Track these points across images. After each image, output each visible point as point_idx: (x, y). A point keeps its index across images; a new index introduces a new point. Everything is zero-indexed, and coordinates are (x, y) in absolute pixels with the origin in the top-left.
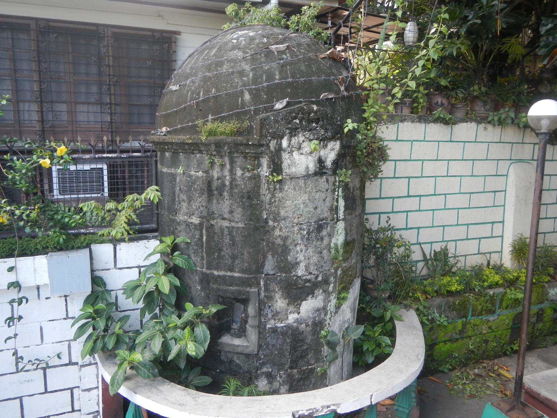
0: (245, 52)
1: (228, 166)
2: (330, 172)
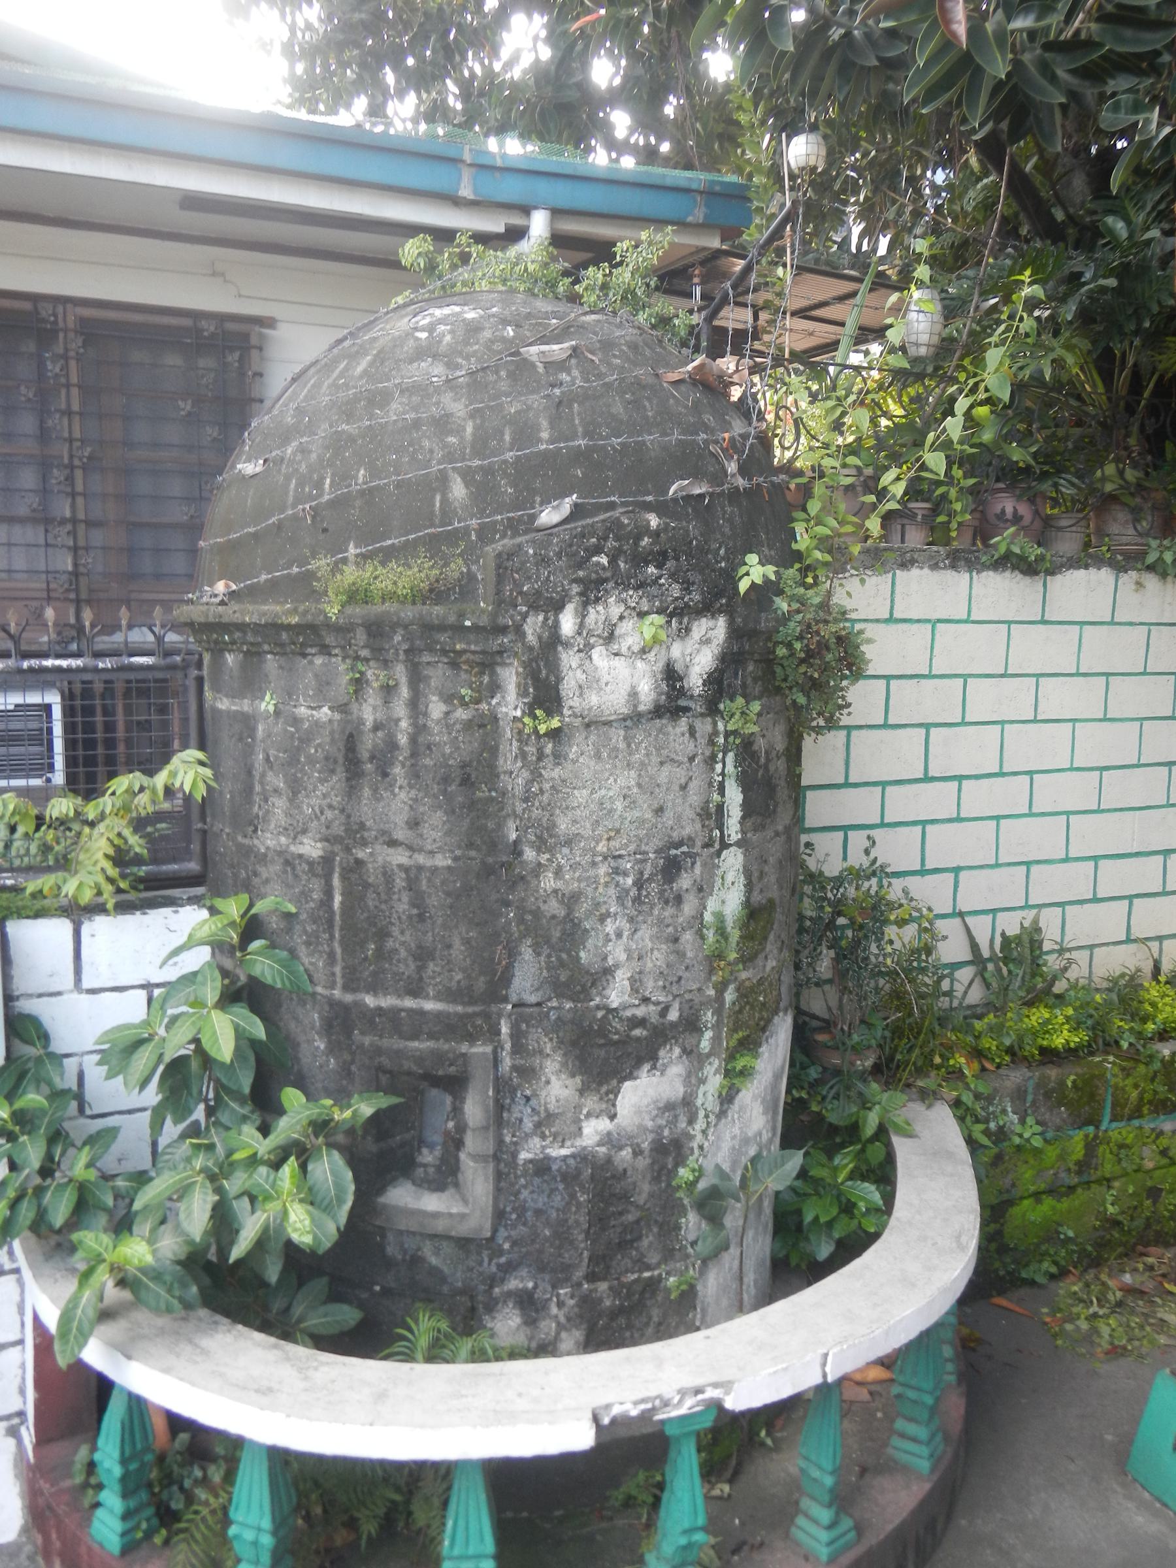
0: (451, 366)
1: (405, 692)
2: (699, 708)
